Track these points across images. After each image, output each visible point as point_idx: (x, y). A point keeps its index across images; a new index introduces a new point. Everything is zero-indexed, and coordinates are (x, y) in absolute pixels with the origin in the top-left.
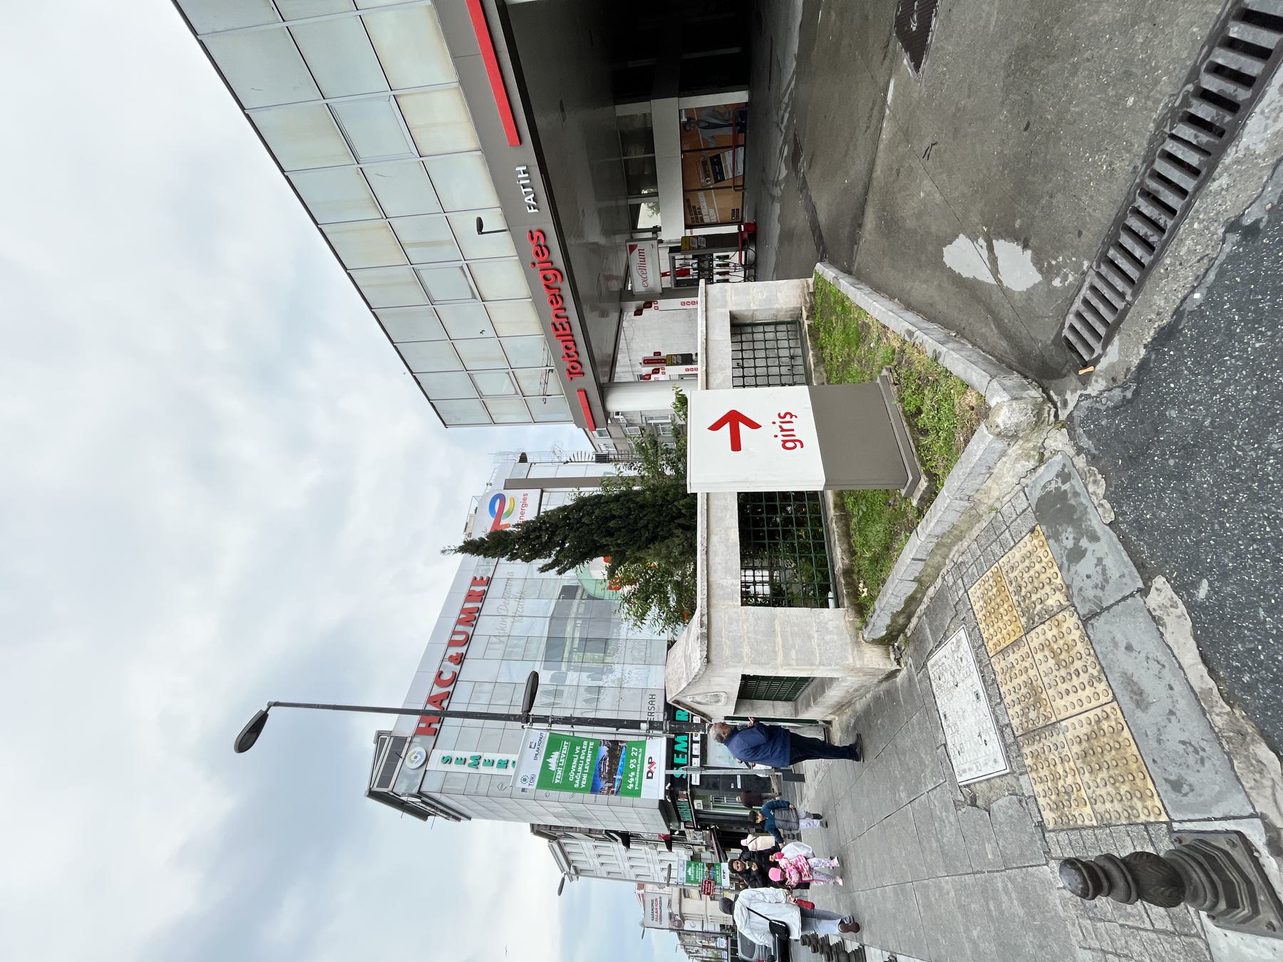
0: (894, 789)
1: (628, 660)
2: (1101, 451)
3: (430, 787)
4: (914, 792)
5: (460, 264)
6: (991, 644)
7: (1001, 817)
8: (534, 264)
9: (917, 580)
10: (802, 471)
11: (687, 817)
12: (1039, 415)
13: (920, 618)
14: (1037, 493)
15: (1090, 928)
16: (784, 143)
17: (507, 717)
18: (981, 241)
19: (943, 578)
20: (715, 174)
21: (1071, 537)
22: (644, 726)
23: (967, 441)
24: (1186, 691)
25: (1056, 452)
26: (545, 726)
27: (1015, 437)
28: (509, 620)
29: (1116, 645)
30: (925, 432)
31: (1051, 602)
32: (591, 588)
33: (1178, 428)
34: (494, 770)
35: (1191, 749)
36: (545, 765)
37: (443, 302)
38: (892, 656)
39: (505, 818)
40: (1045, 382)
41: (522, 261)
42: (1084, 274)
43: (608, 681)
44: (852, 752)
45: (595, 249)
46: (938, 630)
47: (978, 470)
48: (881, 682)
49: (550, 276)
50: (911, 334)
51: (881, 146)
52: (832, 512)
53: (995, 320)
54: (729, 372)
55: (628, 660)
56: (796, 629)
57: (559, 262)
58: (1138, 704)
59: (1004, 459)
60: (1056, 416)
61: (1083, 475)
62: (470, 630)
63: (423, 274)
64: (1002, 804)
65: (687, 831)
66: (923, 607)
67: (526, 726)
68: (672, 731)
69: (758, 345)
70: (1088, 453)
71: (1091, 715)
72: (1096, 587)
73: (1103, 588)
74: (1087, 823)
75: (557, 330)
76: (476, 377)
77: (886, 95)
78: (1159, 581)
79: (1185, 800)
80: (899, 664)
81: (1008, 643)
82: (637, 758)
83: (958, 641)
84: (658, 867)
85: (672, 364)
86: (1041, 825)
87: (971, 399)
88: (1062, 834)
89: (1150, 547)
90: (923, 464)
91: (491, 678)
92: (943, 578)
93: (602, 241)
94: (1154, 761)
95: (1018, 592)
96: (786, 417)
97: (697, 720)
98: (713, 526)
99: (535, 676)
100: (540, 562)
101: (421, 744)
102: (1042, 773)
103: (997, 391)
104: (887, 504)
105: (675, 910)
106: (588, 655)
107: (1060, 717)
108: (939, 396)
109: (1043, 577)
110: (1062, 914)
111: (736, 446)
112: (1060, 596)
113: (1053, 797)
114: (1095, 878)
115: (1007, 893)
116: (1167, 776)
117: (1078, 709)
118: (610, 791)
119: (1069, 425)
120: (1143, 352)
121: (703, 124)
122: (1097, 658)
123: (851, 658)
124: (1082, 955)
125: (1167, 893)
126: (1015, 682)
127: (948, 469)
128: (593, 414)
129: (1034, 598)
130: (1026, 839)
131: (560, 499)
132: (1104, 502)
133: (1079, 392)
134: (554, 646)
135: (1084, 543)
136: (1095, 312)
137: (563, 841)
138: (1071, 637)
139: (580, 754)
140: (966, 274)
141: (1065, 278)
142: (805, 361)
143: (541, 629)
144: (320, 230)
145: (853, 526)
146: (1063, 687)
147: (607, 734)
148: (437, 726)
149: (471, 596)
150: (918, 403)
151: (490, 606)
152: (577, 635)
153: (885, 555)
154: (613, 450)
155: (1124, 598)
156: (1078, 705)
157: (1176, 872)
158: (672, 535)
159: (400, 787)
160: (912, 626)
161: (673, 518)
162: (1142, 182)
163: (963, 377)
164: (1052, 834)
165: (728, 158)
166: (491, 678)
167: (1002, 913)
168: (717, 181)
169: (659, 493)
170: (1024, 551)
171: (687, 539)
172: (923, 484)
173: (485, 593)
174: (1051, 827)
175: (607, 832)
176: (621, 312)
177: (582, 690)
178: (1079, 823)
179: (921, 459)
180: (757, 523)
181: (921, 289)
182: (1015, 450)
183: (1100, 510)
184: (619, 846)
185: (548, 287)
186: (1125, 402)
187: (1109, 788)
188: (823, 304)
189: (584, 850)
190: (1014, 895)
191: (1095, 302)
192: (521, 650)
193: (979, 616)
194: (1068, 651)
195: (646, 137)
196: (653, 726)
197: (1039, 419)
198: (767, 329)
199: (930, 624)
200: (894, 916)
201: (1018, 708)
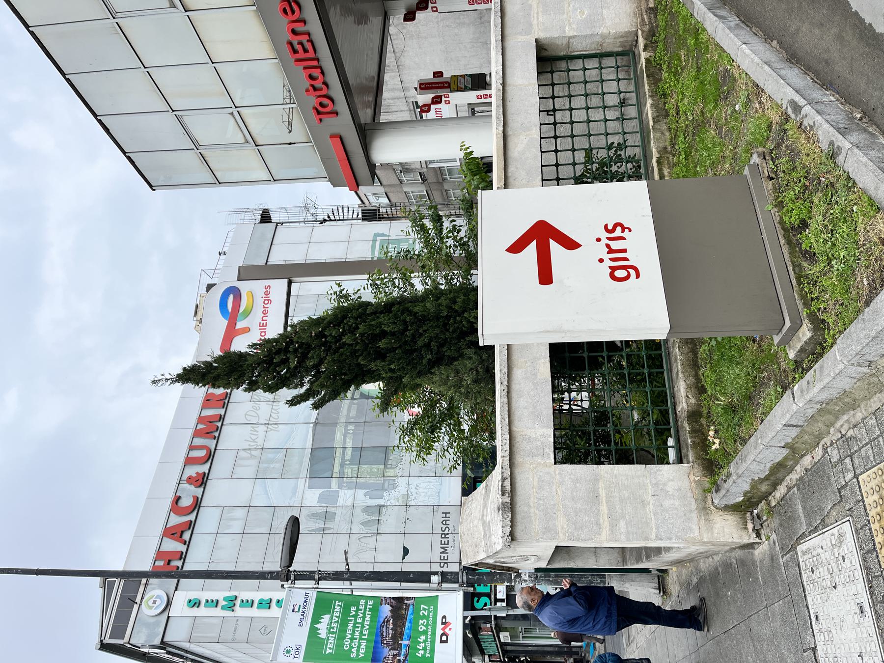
10: (639, 313)
13: (789, 488)
17: (262, 575)
22: (435, 579)
26: (310, 584)
30: (811, 256)
34: (254, 612)
36: (313, 632)
37: (130, 14)
38: (750, 526)
43: (390, 498)
44: (690, 619)
50: (797, 108)
54: (535, 134)
56: (626, 494)
62: (212, 444)
66: (794, 477)
67: (287, 585)
68: (470, 584)
69: (578, 89)
76: (187, 120)
80: (758, 535)
82: (427, 618)
83: (841, 535)
85: (459, 90)
90: (807, 305)
92: (825, 449)
100: (287, 393)
106: (364, 468)
108: (836, 211)
111: (545, 276)
123: (695, 528)
128: (353, 164)
131: (315, 299)
139: (356, 616)
142: (640, 112)
152: (349, 444)
153: (745, 410)
154: (384, 200)
158: (462, 356)
163: (872, 193)
169: (443, 301)
171: (482, 361)
177: (358, 510)
179: (803, 297)
192: (278, 466)
193: (872, 513)
199: (804, 501)
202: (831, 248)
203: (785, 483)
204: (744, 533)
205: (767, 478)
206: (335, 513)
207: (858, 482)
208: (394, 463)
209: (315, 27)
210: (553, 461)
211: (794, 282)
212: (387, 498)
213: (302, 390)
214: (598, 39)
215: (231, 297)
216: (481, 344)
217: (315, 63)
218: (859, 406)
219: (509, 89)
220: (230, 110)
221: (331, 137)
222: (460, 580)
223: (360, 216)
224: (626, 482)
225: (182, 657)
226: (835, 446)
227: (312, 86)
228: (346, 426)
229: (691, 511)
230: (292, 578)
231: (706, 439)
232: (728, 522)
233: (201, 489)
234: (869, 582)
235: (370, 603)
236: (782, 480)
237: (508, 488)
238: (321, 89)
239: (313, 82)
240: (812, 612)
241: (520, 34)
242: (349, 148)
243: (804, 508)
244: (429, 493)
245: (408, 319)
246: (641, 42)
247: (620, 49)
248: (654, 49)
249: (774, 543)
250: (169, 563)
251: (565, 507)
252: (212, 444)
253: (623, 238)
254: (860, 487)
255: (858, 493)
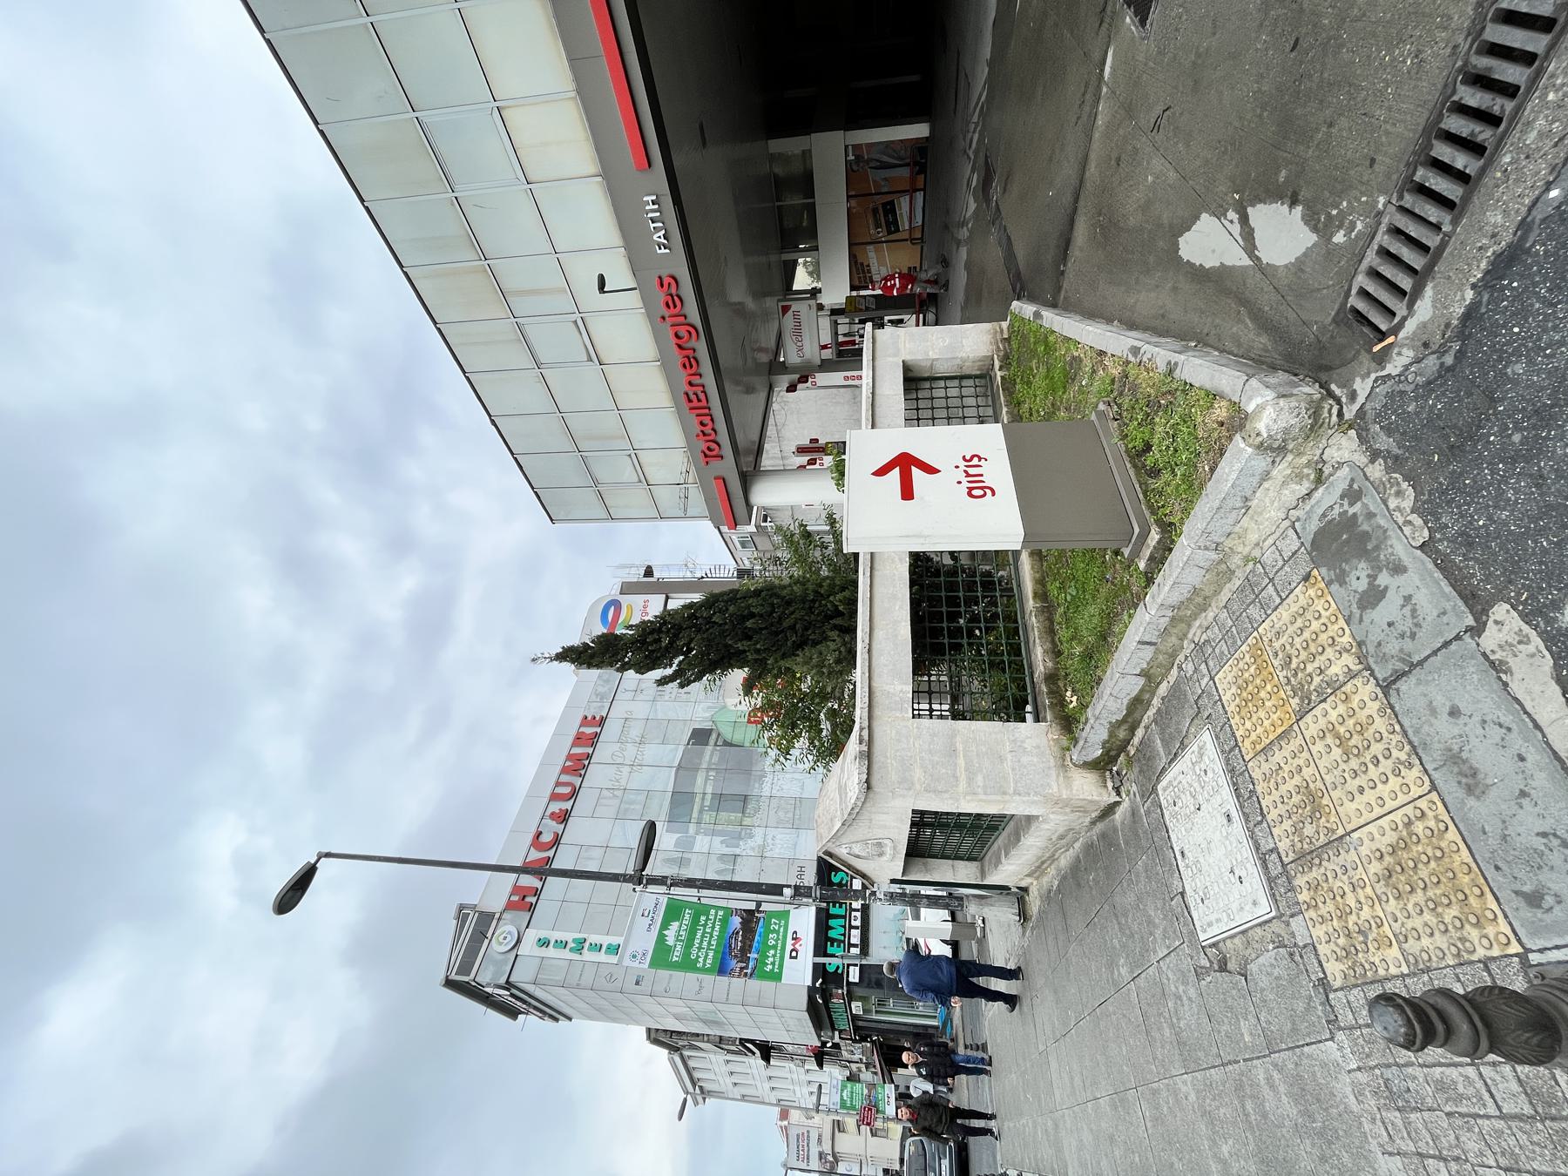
0: (1111, 965)
2: (1407, 449)
3: (521, 977)
4: (1139, 964)
6: (1247, 743)
7: (1264, 982)
9: (1144, 674)
10: (990, 524)
11: (843, 1023)
12: (1316, 415)
13: (1147, 728)
14: (1314, 525)
15: (1399, 1122)
16: (973, 171)
18: (1232, 215)
19: (1180, 668)
20: (888, 224)
21: (1363, 575)
22: (788, 892)
23: (1212, 470)
24: (1546, 759)
25: (1341, 464)
26: (663, 889)
27: (1281, 450)
28: (626, 770)
29: (1434, 712)
31: (1336, 670)
32: (727, 733)
33: (1528, 387)
34: (602, 957)
35: (1556, 842)
36: (661, 938)
38: (1110, 784)
39: (614, 1020)
40: (1324, 377)
41: (649, 315)
42: (1380, 214)
43: (747, 847)
45: (739, 310)
46: (1172, 738)
48: (1093, 823)
49: (683, 333)
51: (1097, 135)
52: (1031, 604)
57: (694, 316)
58: (1470, 790)
59: (1266, 485)
60: (1340, 414)
61: (1379, 488)
62: (577, 781)
63: (528, 330)
64: (1266, 964)
65: (842, 1043)
66: (1151, 712)
67: (638, 888)
70: (1387, 455)
71: (1397, 817)
72: (1402, 636)
73: (1413, 636)
74: (1393, 971)
75: (690, 401)
77: (1102, 70)
78: (1501, 611)
79: (1548, 918)
80: (1119, 794)
81: (1272, 737)
82: (777, 932)
84: (806, 1090)
86: (1324, 984)
87: (1221, 411)
88: (1355, 991)
89: (1483, 565)
90: (1153, 513)
91: (600, 836)
92: (1180, 668)
93: (750, 304)
94: (1497, 868)
95: (1287, 664)
97: (857, 884)
100: (658, 673)
101: (512, 922)
102: (1323, 910)
104: (1103, 578)
105: (827, 1148)
106: (723, 815)
107: (1349, 828)
109: (1323, 638)
110: (1355, 1107)
111: (907, 493)
112: (1349, 660)
113: (1342, 941)
114: (1425, 1021)
115: (1272, 1086)
116: (1518, 887)
117: (1378, 811)
118: (742, 973)
119: (1359, 424)
120: (1469, 295)
121: (873, 164)
122: (1405, 733)
124: (1386, 1164)
125: (1535, 1041)
126: (1283, 789)
127: (1186, 512)
128: (731, 506)
129: (1310, 668)
130: (1300, 1006)
132: (1415, 518)
133: (1373, 376)
134: (681, 801)
135: (1384, 579)
136: (1396, 260)
137: (686, 1053)
138: (1366, 712)
139: (705, 926)
140: (1210, 263)
141: (1353, 226)
143: (666, 781)
144: (406, 274)
145: (1057, 618)
146: (1353, 785)
147: (745, 901)
148: (533, 900)
149: (579, 739)
151: (603, 752)
152: (709, 790)
153: (1105, 640)
155: (1446, 644)
156: (1378, 804)
157: (1538, 1008)
158: (826, 639)
159: (486, 975)
160: (1136, 740)
161: (828, 618)
162: (1466, 63)
163: (1208, 386)
164: (1340, 994)
165: (903, 205)
166: (600, 836)
167: (1265, 1116)
168: (890, 233)
169: (810, 587)
170: (1294, 608)
171: (844, 644)
173: (597, 735)
174: (1337, 984)
175: (743, 1041)
176: (771, 388)
177: (713, 858)
178: (1381, 972)
179: (1150, 507)
180: (936, 633)
181: (1146, 300)
182: (1282, 469)
183: (1407, 530)
184: (756, 1061)
185: (680, 347)
186: (1445, 371)
187: (1427, 916)
188: (1021, 349)
189: (713, 1064)
190: (1282, 1089)
191: (1388, 271)
192: (639, 807)
193: (1231, 708)
194: (1360, 733)
195: (805, 183)
196: (799, 892)
197: (1316, 421)
199: (1162, 732)
200: (1111, 1138)
201: (1287, 825)
204: (1103, 791)
209: (709, 380)
213: (669, 671)
214: (959, 362)
225: (525, 1002)
235: (721, 913)
240: (1177, 849)
246: (997, 364)
252: (577, 781)
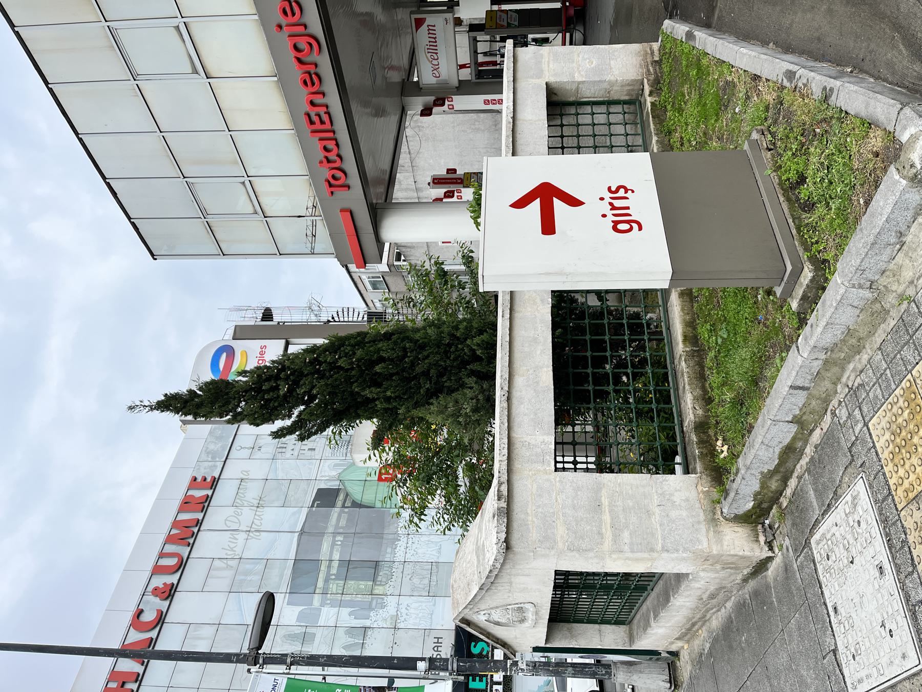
1: (406, 590)
5: (175, 22)
6: (900, 491)
8: (280, 27)
9: (797, 420)
10: (639, 262)
13: (800, 478)
19: (833, 414)
22: (422, 665)
23: (867, 203)
26: (282, 668)
28: (241, 537)
37: (150, 77)
38: (762, 539)
41: (264, 22)
43: (378, 619)
46: (826, 488)
47: (885, 238)
48: (745, 580)
49: (303, 45)
52: (680, 347)
53: (904, 38)
55: (406, 590)
57: (316, 27)
63: (123, 36)
66: (804, 461)
67: (254, 669)
68: (459, 672)
69: (583, 130)
75: (312, 123)
80: (771, 549)
90: (807, 249)
92: (833, 414)
96: (618, 191)
98: (517, 364)
99: (269, 601)
103: (911, 119)
104: (755, 320)
111: (548, 227)
127: (840, 248)
128: (359, 244)
134: (304, 570)
143: (286, 548)
145: (708, 363)
149: (187, 504)
150: (801, 168)
151: (216, 517)
152: (336, 556)
158: (463, 386)
160: (789, 492)
161: (464, 363)
163: (863, 114)
171: (482, 391)
172: (807, 274)
173: (208, 499)
176: (403, 112)
177: (341, 632)
179: (804, 243)
185: (299, 60)
188: (673, 73)
193: (885, 455)
198: (596, 109)
202: (828, 187)
203: (795, 474)
204: (755, 546)
205: (776, 470)
206: (314, 634)
207: (868, 429)
208: (384, 580)
210: (553, 468)
211: (794, 232)
212: (374, 619)
214: (606, 86)
215: (224, 356)
216: (481, 290)
217: (330, 135)
218: (864, 347)
219: (518, 123)
220: (242, 180)
221: (342, 211)
222: (450, 667)
223: (365, 319)
224: (630, 492)
226: (843, 404)
227: (326, 157)
228: (334, 537)
229: (699, 522)
230: (261, 661)
231: (715, 450)
232: (738, 535)
233: (167, 602)
234: (887, 535)
236: (793, 472)
237: (505, 493)
238: (335, 162)
239: (327, 154)
241: (532, 78)
242: (358, 224)
243: (815, 491)
244: (420, 615)
245: (407, 345)
247: (627, 98)
248: (659, 95)
249: (788, 549)
250: (122, 686)
251: (564, 515)
253: (626, 198)
254: (870, 434)
255: (869, 440)
